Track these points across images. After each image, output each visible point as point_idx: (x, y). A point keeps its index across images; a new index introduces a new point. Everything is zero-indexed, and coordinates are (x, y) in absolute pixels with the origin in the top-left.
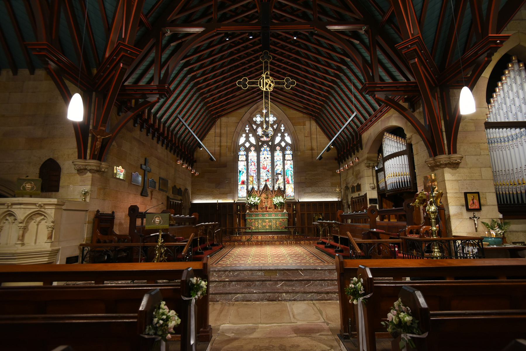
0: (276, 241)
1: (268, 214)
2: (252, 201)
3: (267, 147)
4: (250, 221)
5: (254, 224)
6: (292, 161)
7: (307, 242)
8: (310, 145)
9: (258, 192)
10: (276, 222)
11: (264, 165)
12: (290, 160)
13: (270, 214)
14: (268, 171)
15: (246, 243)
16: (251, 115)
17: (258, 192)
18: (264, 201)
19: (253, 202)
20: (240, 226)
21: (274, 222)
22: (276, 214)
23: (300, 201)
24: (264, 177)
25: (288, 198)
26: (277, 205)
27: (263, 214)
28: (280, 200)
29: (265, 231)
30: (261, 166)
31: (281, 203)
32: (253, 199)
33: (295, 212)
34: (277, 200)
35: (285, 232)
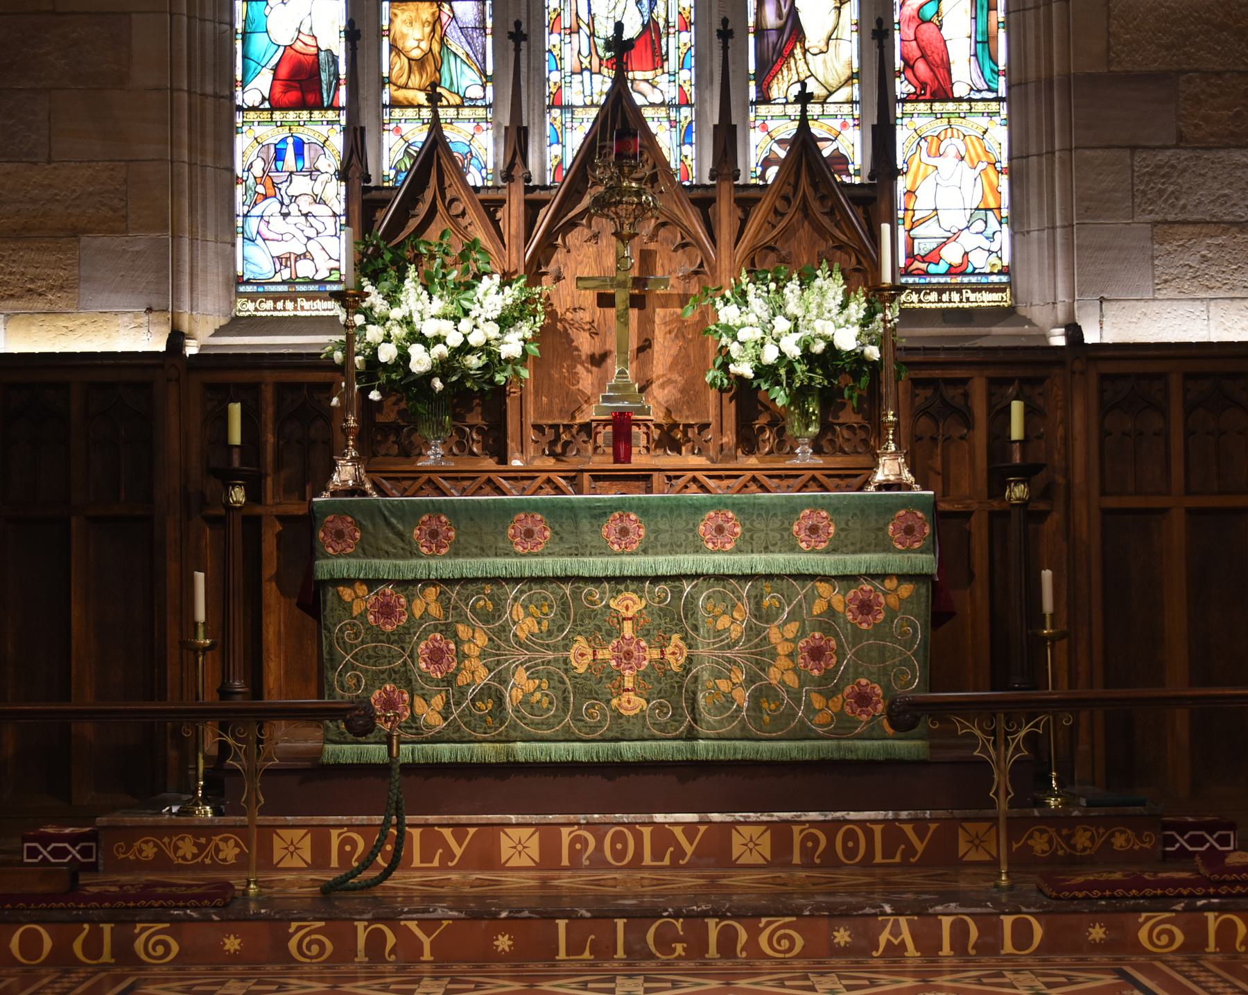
0: (751, 915)
1: (644, 510)
2: (420, 338)
5: (436, 656)
13: (674, 509)
17: (512, 216)
18: (585, 344)
19: (440, 350)
21: (734, 624)
22: (766, 511)
25: (931, 300)
26: (780, 397)
27: (572, 511)
29: (601, 751)
32: (438, 306)
33: (1018, 492)
34: (781, 324)
35: (893, 764)
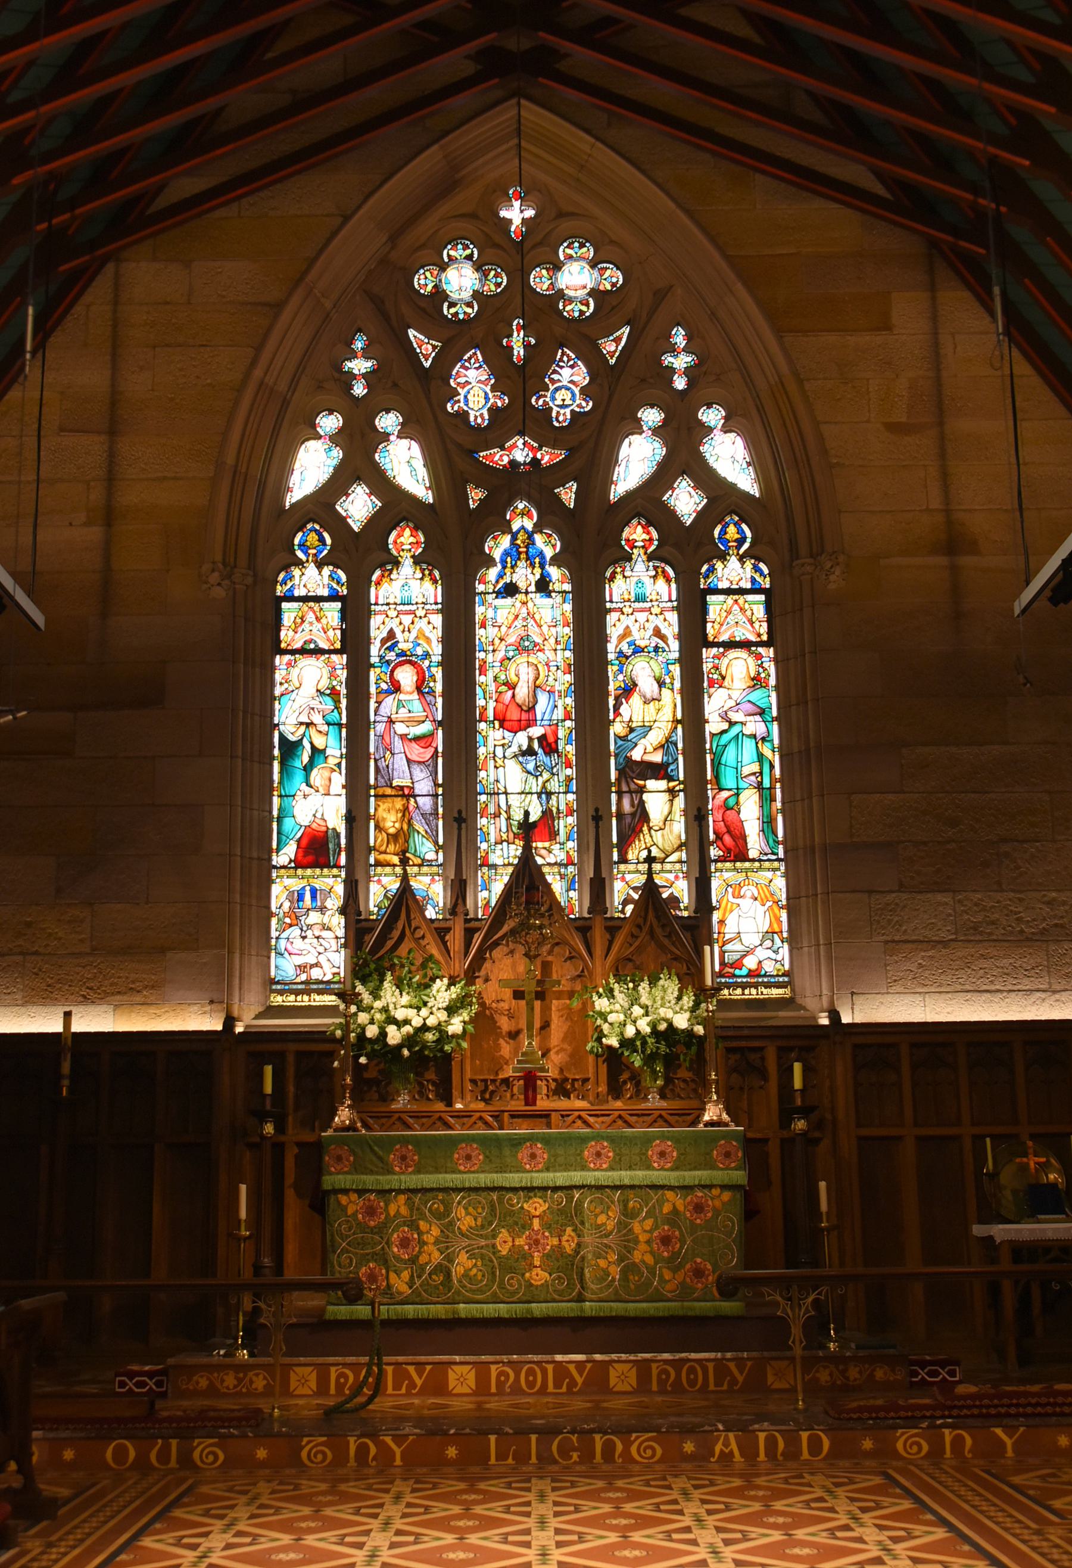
0: (624, 1431)
1: (547, 1141)
2: (392, 1021)
3: (538, 528)
4: (371, 1211)
5: (405, 1243)
6: (768, 653)
7: (958, 1442)
8: (936, 503)
9: (456, 939)
10: (621, 1225)
11: (512, 687)
12: (745, 645)
13: (567, 1140)
14: (549, 745)
15: (312, 1448)
16: (393, 239)
17: (456, 939)
20: (279, 1269)
21: (609, 1220)
22: (631, 1140)
23: (846, 1019)
24: (515, 801)
26: (637, 1061)
27: (497, 1141)
28: (663, 1012)
30: (485, 702)
31: (669, 1034)
33: (800, 1125)
34: (637, 1011)
